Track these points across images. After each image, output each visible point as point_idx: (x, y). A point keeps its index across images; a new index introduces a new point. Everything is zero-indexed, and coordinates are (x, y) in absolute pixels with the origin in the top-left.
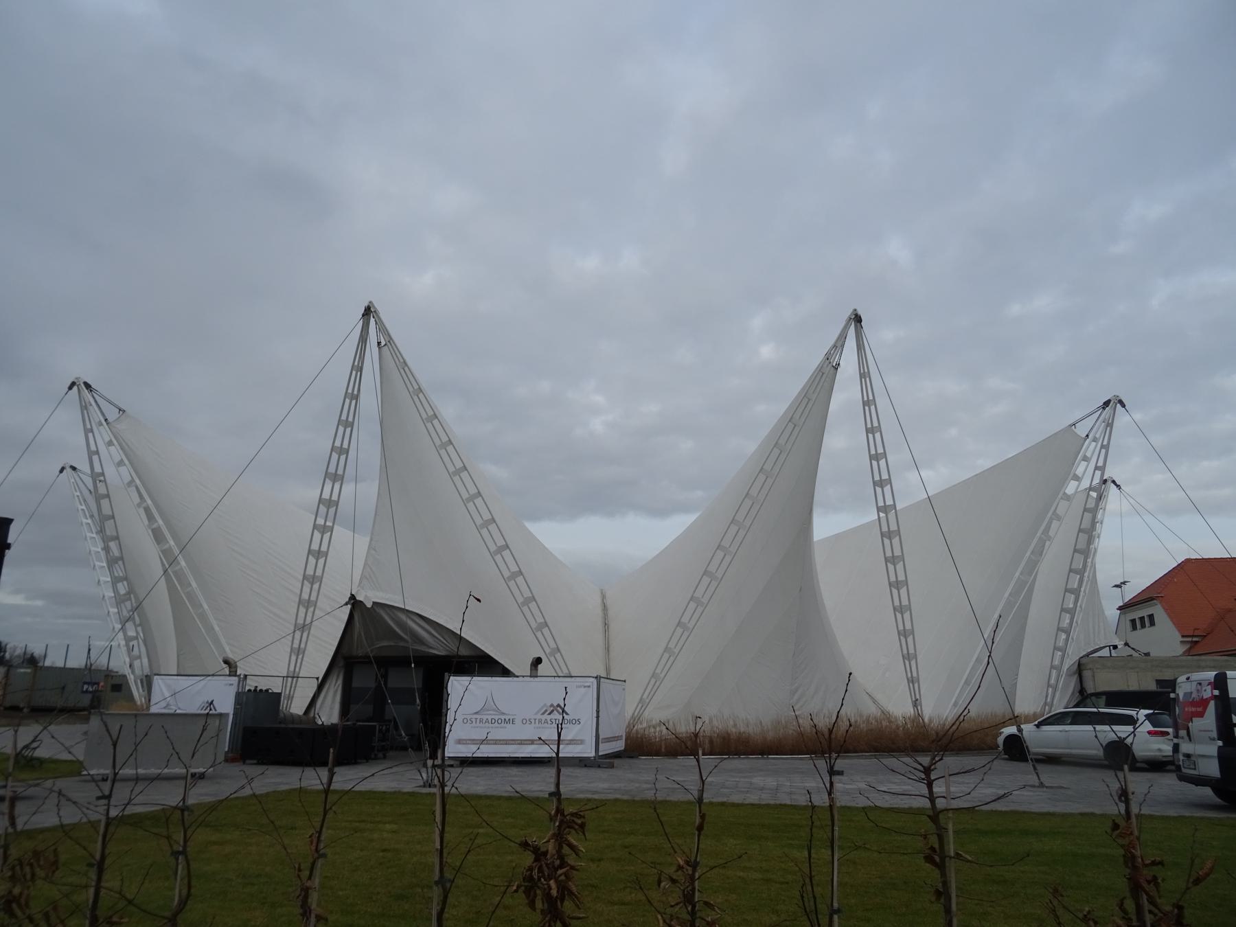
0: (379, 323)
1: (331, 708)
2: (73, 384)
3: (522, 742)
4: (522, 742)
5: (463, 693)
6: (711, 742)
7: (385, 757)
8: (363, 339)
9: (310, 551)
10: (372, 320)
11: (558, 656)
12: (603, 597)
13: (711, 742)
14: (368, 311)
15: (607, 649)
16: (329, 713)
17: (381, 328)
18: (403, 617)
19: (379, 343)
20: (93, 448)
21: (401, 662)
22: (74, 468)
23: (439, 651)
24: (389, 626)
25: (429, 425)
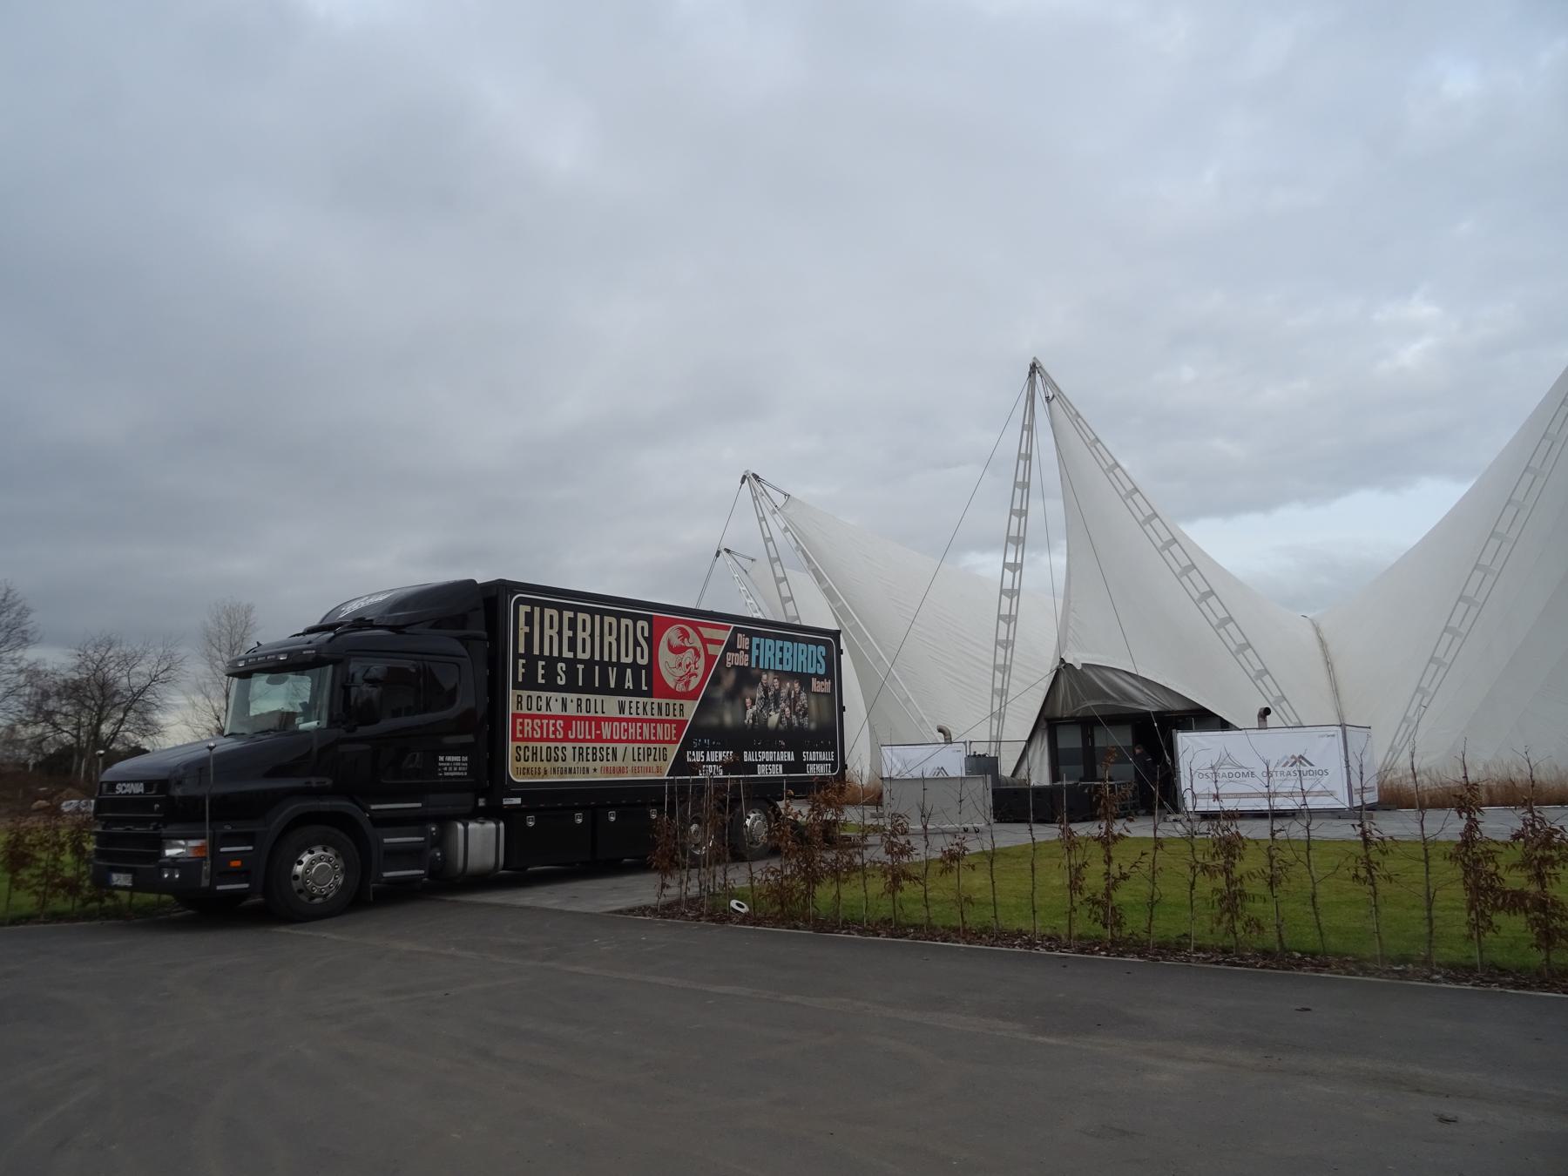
1: (1041, 770)
3: (1248, 795)
4: (1248, 795)
5: (1192, 747)
6: (1489, 791)
8: (1031, 397)
9: (999, 617)
11: (1284, 704)
12: (1317, 630)
13: (1489, 791)
14: (1034, 368)
15: (1336, 692)
16: (1039, 774)
17: (1049, 382)
18: (1111, 675)
21: (1116, 719)
22: (728, 551)
23: (1151, 708)
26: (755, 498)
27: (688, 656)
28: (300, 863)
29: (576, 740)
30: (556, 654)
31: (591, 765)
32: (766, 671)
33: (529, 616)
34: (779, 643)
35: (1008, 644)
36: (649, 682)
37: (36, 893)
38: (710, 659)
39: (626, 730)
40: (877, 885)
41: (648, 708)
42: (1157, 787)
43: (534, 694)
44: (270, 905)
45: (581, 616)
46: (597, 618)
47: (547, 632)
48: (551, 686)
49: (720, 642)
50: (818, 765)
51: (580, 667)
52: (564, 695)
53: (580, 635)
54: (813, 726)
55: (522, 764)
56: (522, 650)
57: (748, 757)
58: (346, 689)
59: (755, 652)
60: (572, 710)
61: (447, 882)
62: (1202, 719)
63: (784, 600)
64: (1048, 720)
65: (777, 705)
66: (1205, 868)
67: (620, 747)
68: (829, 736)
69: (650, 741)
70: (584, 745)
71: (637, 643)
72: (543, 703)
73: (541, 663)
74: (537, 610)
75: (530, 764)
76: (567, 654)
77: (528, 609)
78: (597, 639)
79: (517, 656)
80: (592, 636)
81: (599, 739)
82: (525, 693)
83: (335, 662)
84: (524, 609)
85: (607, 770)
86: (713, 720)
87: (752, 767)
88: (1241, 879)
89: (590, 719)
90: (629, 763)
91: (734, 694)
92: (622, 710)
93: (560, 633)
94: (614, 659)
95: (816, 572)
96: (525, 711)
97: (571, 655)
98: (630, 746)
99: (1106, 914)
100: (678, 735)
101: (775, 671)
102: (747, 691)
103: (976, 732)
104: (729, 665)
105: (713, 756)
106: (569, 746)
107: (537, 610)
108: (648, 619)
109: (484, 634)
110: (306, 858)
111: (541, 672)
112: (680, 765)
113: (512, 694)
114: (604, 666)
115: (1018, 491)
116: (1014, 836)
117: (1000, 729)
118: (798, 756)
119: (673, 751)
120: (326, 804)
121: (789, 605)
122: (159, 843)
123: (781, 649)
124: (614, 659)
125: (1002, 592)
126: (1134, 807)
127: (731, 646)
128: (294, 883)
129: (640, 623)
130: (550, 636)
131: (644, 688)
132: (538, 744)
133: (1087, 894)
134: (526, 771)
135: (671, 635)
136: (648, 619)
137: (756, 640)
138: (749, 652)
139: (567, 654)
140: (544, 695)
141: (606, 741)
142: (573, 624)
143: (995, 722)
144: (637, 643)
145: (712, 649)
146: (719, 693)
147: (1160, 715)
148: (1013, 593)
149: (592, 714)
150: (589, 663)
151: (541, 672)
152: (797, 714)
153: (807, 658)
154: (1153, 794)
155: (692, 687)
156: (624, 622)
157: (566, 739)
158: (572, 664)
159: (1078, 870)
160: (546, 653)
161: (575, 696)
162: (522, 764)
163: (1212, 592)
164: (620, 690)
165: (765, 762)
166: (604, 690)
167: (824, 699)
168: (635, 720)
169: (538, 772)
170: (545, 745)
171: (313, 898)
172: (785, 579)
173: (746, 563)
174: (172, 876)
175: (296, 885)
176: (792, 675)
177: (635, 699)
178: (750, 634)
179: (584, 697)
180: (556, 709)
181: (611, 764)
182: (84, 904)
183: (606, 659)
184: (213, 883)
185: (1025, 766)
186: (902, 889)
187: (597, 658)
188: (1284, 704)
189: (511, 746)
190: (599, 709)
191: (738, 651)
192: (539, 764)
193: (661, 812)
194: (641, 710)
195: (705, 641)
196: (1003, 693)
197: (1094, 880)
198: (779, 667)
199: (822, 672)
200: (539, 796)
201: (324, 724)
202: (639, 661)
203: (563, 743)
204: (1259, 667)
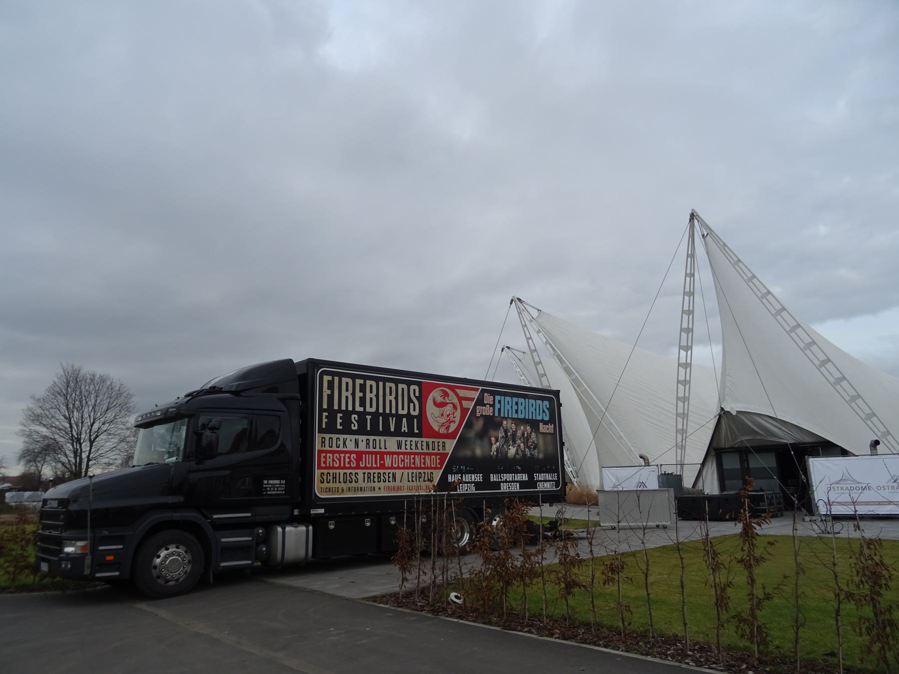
0: (701, 221)
1: (712, 484)
2: (512, 300)
3: (880, 503)
4: (880, 503)
5: (820, 469)
7: (782, 515)
8: (692, 236)
9: (678, 382)
10: (696, 221)
11: (889, 437)
14: (693, 216)
16: (711, 487)
17: (704, 224)
19: (703, 235)
20: (528, 336)
21: (764, 449)
22: (509, 348)
23: (788, 440)
24: (750, 427)
25: (750, 284)
26: (519, 313)
27: (448, 409)
28: (159, 557)
29: (366, 468)
30: (350, 408)
31: (377, 485)
32: (506, 418)
33: (331, 385)
34: (515, 399)
35: (685, 399)
36: (419, 426)
37: (7, 572)
38: (464, 411)
39: (403, 461)
40: (553, 590)
41: (419, 445)
42: (796, 496)
43: (334, 436)
44: (133, 585)
45: (369, 383)
46: (381, 384)
47: (344, 394)
48: (347, 430)
49: (472, 399)
50: (546, 483)
51: (369, 417)
52: (357, 437)
53: (368, 395)
54: (541, 456)
55: (325, 485)
56: (325, 406)
57: (494, 478)
58: (199, 436)
59: (497, 406)
60: (362, 447)
61: (273, 568)
62: (827, 448)
63: (541, 376)
64: (715, 450)
65: (514, 441)
66: (850, 596)
67: (398, 473)
68: (553, 462)
69: (421, 468)
70: (372, 471)
71: (410, 401)
72: (341, 443)
73: (339, 415)
74: (336, 379)
75: (331, 485)
76: (359, 409)
77: (330, 378)
78: (381, 398)
79: (321, 410)
80: (377, 396)
81: (383, 466)
82: (327, 436)
83: (190, 416)
84: (326, 378)
85: (389, 489)
86: (468, 453)
87: (497, 485)
88: (890, 609)
89: (376, 453)
90: (405, 483)
91: (483, 435)
92: (399, 446)
93: (353, 394)
94: (394, 412)
95: (559, 357)
96: (327, 448)
97: (361, 409)
98: (406, 471)
99: (752, 632)
100: (441, 464)
101: (513, 419)
102: (492, 432)
103: (668, 461)
104: (478, 414)
105: (467, 478)
106: (360, 472)
107: (336, 379)
108: (418, 384)
109: (298, 395)
110: (163, 553)
111: (339, 421)
112: (444, 484)
113: (318, 437)
114: (386, 417)
115: (687, 298)
116: (692, 532)
117: (683, 456)
118: (531, 477)
119: (437, 475)
120: (177, 515)
121: (544, 379)
122: (60, 543)
123: (517, 403)
124: (394, 412)
125: (679, 365)
126: (780, 510)
127: (480, 402)
128: (153, 571)
129: (412, 387)
130: (346, 396)
131: (416, 431)
132: (338, 471)
133: (733, 613)
134: (329, 490)
135: (436, 394)
136: (418, 384)
137: (498, 398)
138: (493, 406)
139: (359, 409)
140: (342, 437)
141: (388, 468)
142: (363, 388)
143: (679, 451)
144: (410, 401)
145: (465, 404)
146: (472, 434)
147: (795, 446)
148: (687, 365)
149: (377, 449)
150: (375, 415)
151: (339, 421)
152: (529, 448)
153: (537, 410)
154: (793, 502)
155: (451, 430)
156: (400, 386)
157: (358, 467)
158: (362, 416)
159: (723, 590)
160: (343, 408)
161: (364, 438)
162: (325, 485)
163: (829, 360)
164: (398, 433)
165: (506, 481)
166: (387, 432)
167: (549, 437)
168: (410, 454)
169: (337, 490)
170: (342, 472)
171: (167, 581)
172: (541, 362)
173: (520, 355)
174: (66, 566)
175: (155, 573)
176: (525, 421)
177: (409, 439)
178: (493, 394)
179: (371, 438)
180: (351, 446)
181: (392, 484)
182: (41, 580)
183: (388, 411)
184: (94, 570)
185: (701, 481)
186: (574, 595)
187: (381, 411)
188: (889, 437)
189: (317, 473)
190: (382, 446)
191: (485, 405)
192: (338, 485)
193: (400, 520)
194: (413, 447)
195: (460, 399)
196: (683, 432)
197: (738, 599)
198: (515, 416)
199: (547, 418)
200: (336, 507)
201: (180, 459)
202: (412, 413)
203: (348, 469)
204: (868, 411)
